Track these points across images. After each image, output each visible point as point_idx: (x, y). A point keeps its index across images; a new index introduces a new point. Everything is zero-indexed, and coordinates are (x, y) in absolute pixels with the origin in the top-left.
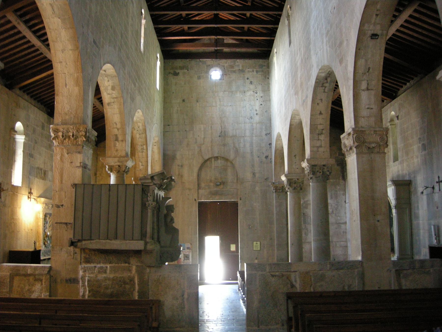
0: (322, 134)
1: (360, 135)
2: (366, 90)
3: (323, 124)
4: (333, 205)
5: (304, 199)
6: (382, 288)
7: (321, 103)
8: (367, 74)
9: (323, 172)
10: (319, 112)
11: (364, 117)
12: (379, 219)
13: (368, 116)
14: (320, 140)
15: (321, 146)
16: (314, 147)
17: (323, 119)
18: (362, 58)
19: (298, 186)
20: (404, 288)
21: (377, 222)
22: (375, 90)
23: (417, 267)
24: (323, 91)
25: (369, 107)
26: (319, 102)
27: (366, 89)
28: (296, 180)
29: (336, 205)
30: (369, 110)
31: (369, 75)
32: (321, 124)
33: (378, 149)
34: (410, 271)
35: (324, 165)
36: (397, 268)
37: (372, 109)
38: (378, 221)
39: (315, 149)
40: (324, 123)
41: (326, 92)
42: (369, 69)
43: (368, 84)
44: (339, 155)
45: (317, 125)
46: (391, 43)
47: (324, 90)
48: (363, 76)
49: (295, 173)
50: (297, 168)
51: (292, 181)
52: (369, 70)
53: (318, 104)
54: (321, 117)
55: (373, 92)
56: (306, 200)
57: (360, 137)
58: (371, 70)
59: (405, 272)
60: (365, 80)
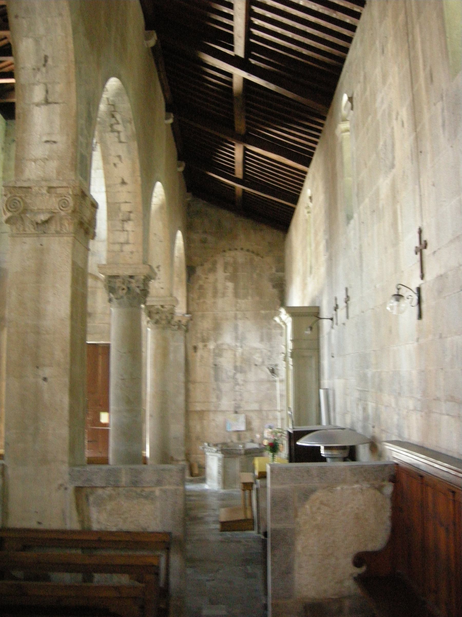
0: (129, 219)
1: (16, 196)
2: (42, 104)
3: (130, 203)
4: (265, 351)
5: (216, 340)
6: (46, 525)
7: (120, 162)
8: (44, 70)
9: (128, 288)
10: (120, 181)
11: (35, 161)
12: (46, 376)
13: (46, 157)
14: (127, 231)
15: (127, 243)
16: (114, 243)
17: (129, 192)
18: (27, 36)
19: (164, 317)
20: (95, 527)
21: (41, 382)
22: (64, 103)
23: (123, 483)
24: (116, 140)
25: (48, 139)
26: (116, 160)
27: (43, 102)
28: (160, 307)
29: (270, 351)
30: (48, 145)
31: (47, 72)
32: (126, 202)
33: (59, 225)
34: (109, 491)
35: (131, 277)
36: (79, 484)
37: (55, 142)
38: (45, 379)
39: (117, 247)
40: (131, 201)
41: (123, 142)
42: (46, 60)
43: (47, 92)
44: (277, 271)
45: (119, 203)
46: (271, 60)
47: (119, 137)
48: (35, 76)
49: (157, 297)
50: (162, 288)
51: (152, 309)
52: (46, 61)
53: (115, 165)
54: (124, 189)
55: (57, 108)
56: (219, 342)
57: (15, 199)
58: (50, 62)
59: (100, 491)
60: (39, 83)
